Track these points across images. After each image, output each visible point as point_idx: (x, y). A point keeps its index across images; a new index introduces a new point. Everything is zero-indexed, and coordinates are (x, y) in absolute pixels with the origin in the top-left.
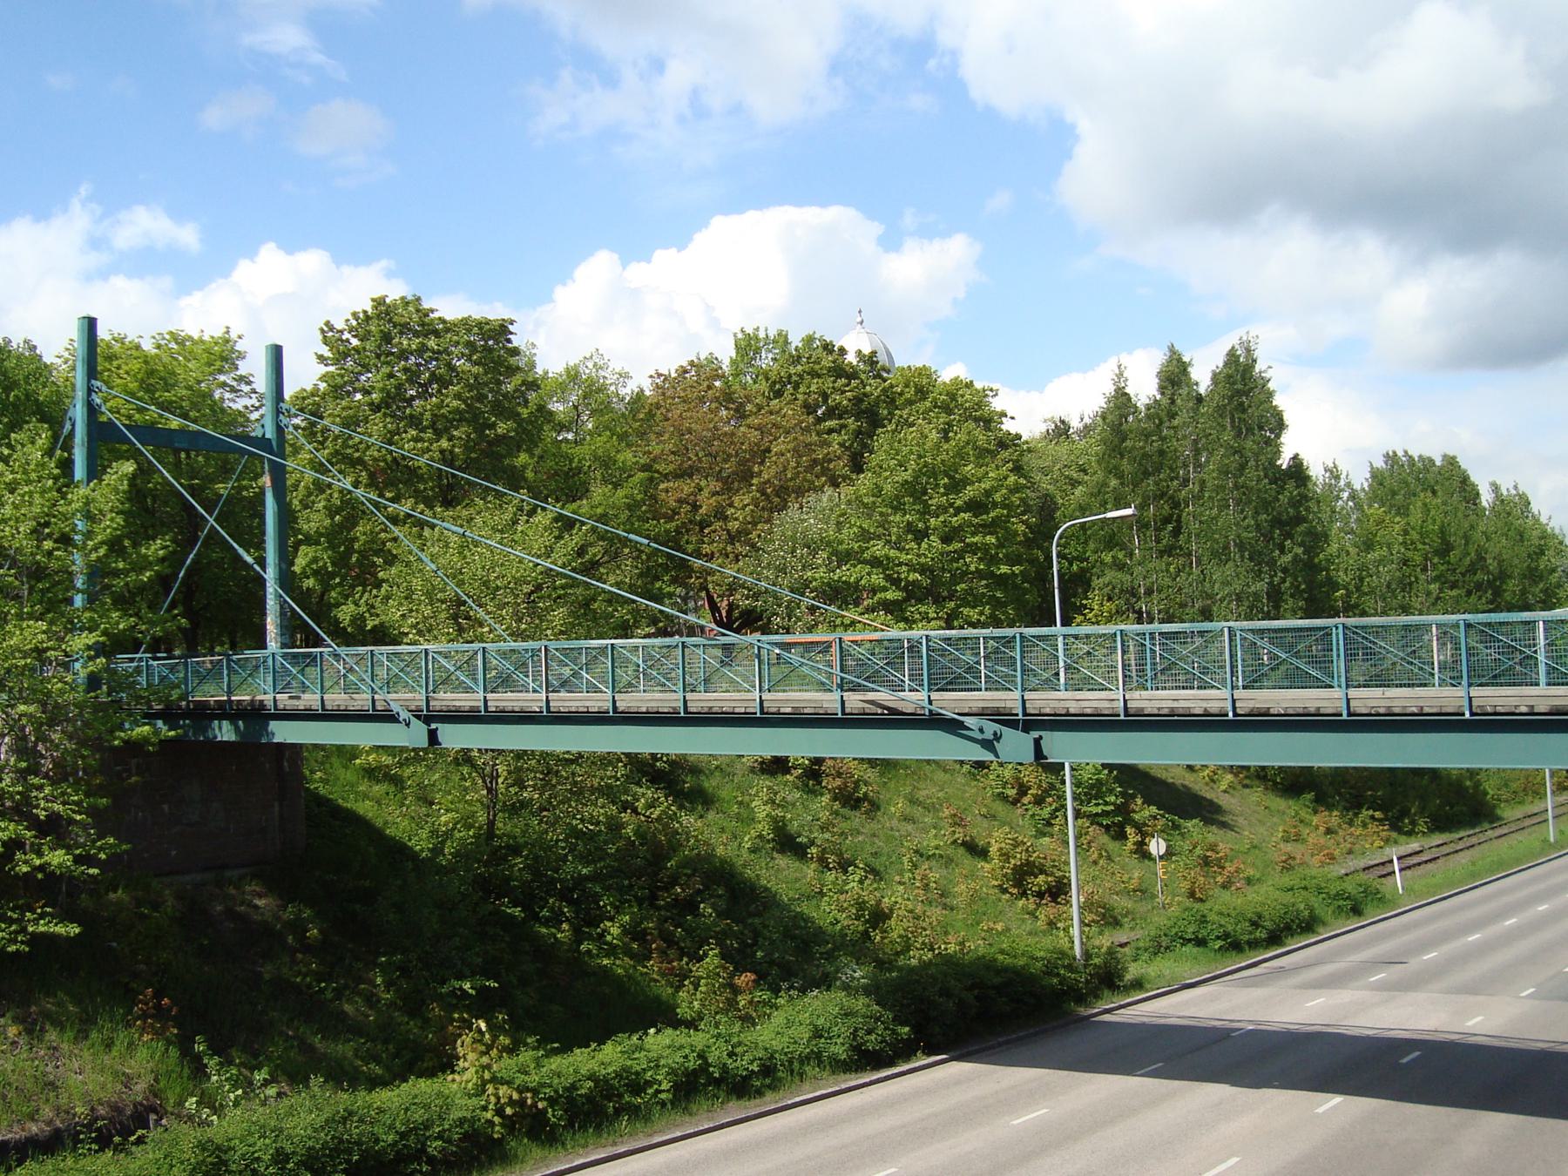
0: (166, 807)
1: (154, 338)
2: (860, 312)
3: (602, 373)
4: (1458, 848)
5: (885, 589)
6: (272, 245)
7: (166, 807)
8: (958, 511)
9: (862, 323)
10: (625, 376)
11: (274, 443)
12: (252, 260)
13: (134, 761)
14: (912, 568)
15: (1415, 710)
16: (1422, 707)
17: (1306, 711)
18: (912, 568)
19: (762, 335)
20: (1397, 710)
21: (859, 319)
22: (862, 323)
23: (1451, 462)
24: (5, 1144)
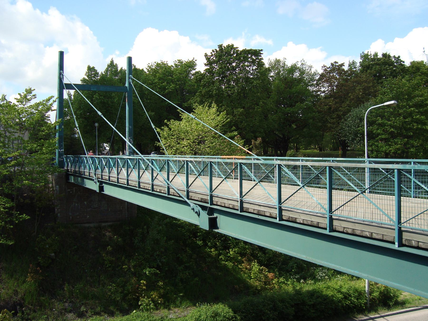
0: (86, 203)
1: (174, 62)
2: (424, 48)
3: (304, 66)
4: (411, 306)
5: (382, 134)
6: (291, 43)
7: (86, 203)
8: (410, 107)
9: (424, 52)
10: (311, 67)
11: (128, 88)
12: (159, 31)
13: (74, 188)
14: (391, 126)
15: (368, 235)
16: (372, 233)
17: (312, 224)
18: (391, 126)
19: (369, 54)
20: (358, 233)
21: (424, 51)
22: (424, 52)
23: (170, 31)
24: (427, 199)
